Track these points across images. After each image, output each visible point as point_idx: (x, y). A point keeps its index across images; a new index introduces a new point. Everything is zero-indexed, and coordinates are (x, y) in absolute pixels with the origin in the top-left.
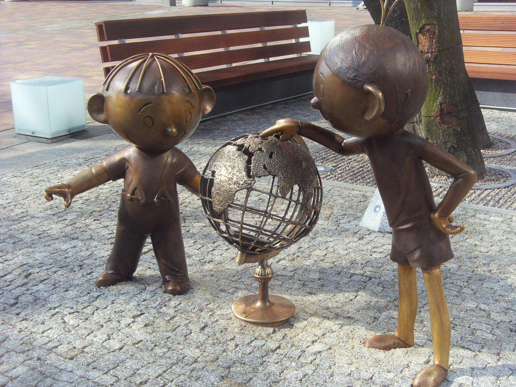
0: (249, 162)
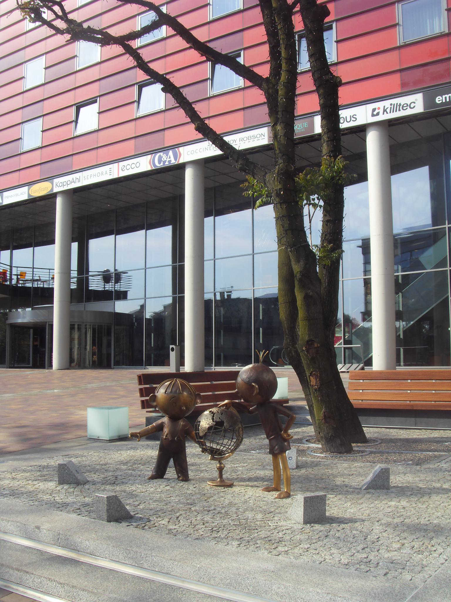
0: (213, 416)
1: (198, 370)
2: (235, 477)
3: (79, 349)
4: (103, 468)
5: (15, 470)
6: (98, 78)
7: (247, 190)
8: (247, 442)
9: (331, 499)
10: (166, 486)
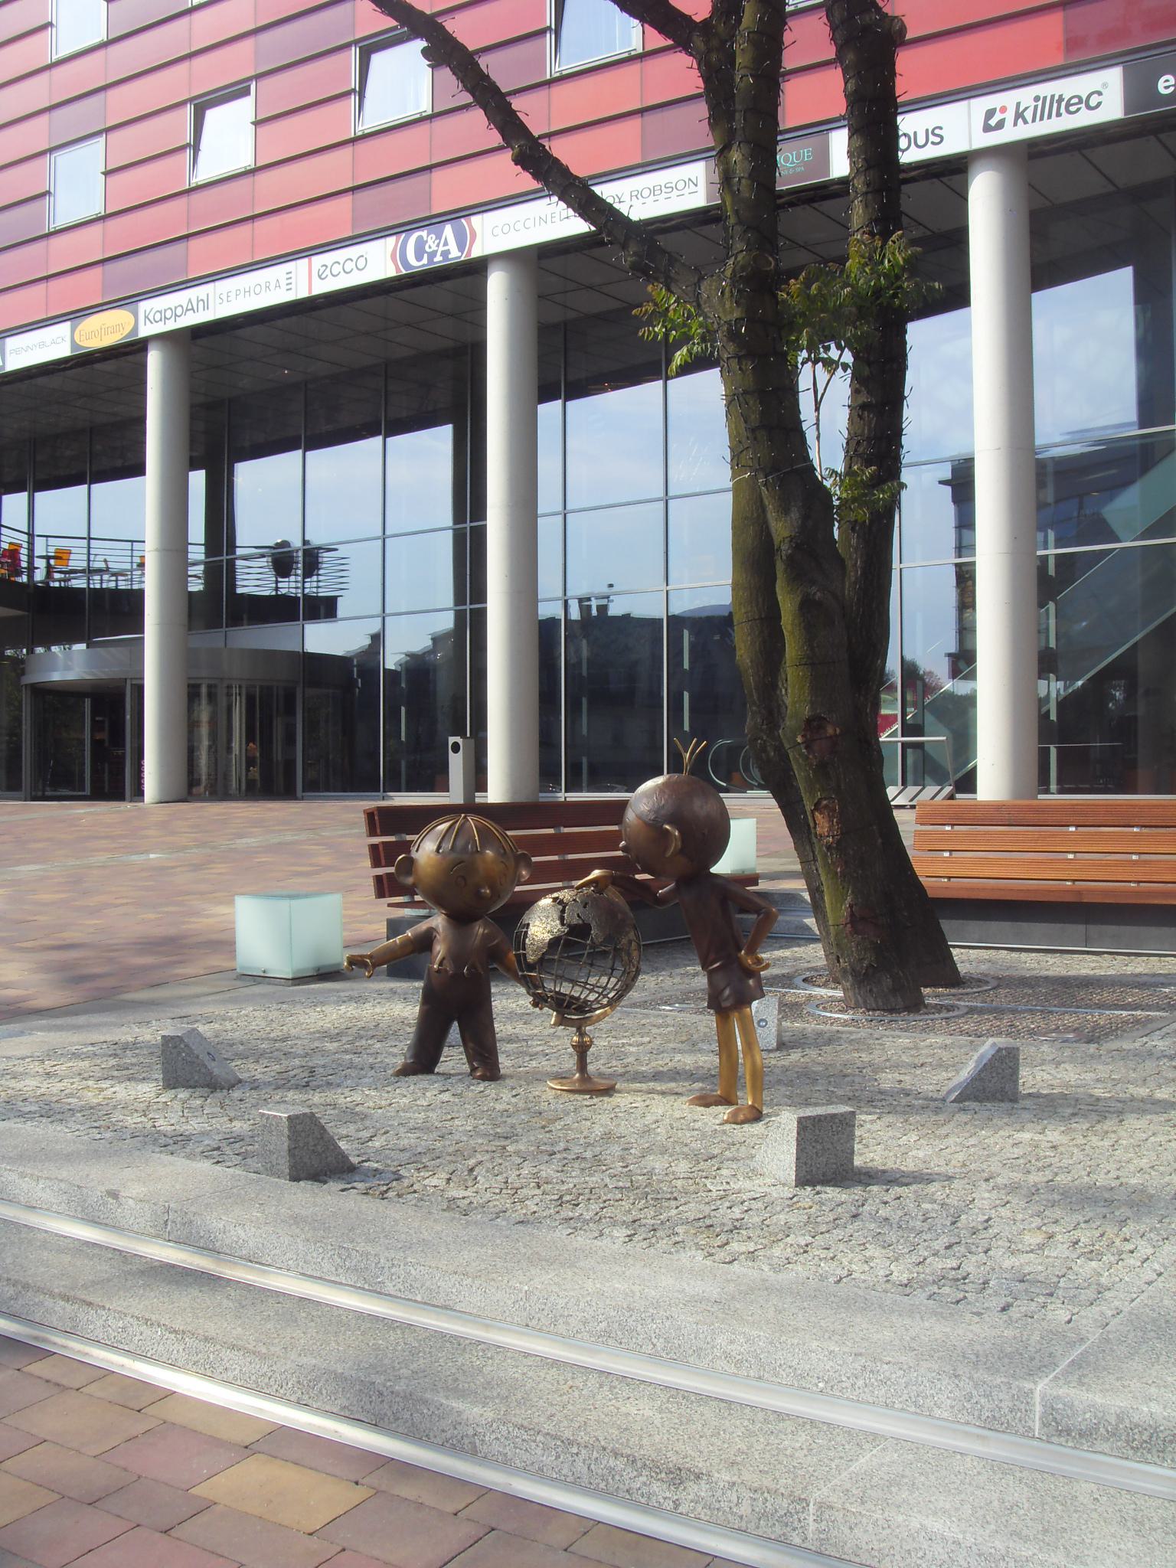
0: (563, 911)
1: (521, 798)
2: (621, 1070)
3: (213, 749)
4: (278, 1048)
5: (52, 1053)
6: (252, 27)
7: (650, 323)
8: (648, 983)
9: (868, 1126)
10: (441, 1092)
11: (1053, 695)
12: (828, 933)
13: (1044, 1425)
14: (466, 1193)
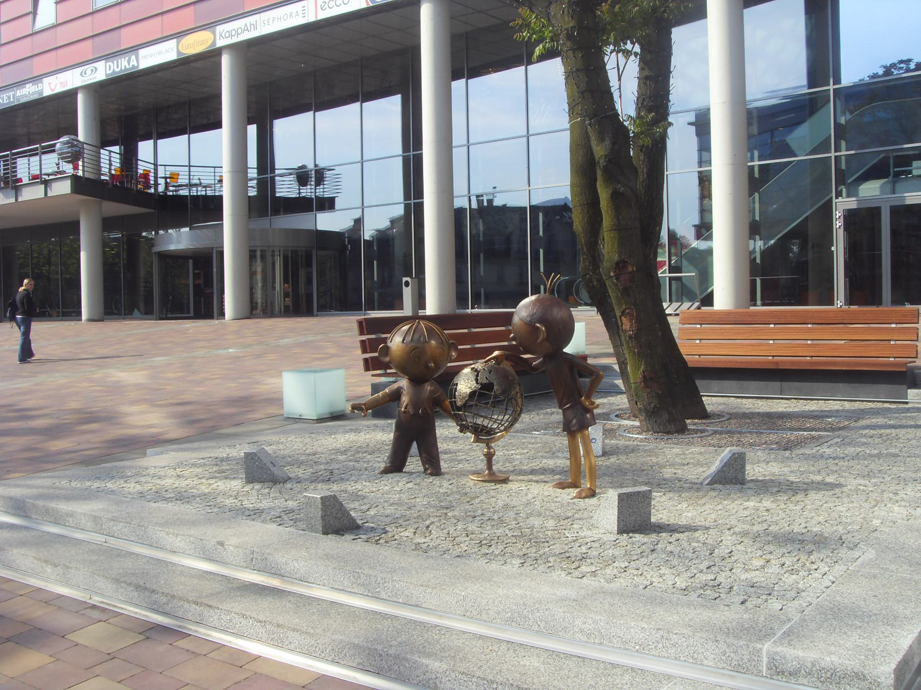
0: (477, 376)
1: (446, 312)
2: (512, 469)
4: (310, 459)
5: (180, 464)
8: (525, 418)
9: (658, 499)
11: (757, 249)
12: (630, 388)
13: (769, 669)
14: (425, 540)
